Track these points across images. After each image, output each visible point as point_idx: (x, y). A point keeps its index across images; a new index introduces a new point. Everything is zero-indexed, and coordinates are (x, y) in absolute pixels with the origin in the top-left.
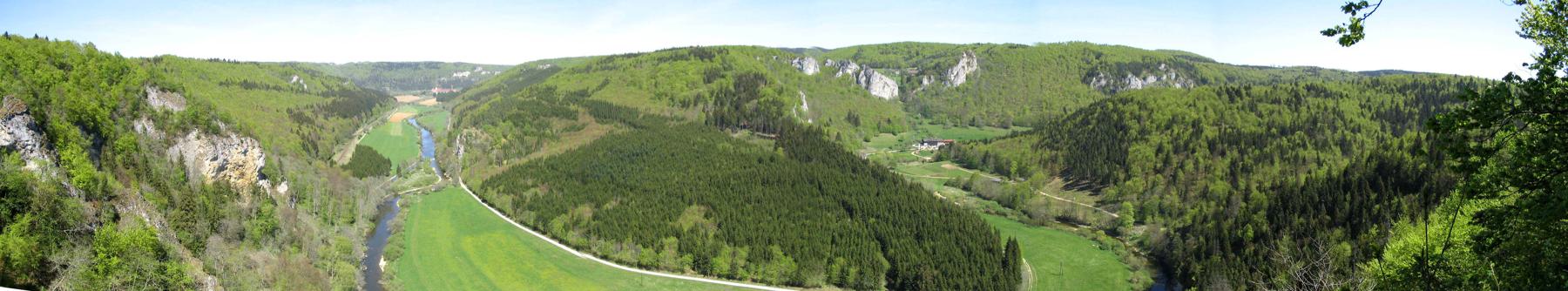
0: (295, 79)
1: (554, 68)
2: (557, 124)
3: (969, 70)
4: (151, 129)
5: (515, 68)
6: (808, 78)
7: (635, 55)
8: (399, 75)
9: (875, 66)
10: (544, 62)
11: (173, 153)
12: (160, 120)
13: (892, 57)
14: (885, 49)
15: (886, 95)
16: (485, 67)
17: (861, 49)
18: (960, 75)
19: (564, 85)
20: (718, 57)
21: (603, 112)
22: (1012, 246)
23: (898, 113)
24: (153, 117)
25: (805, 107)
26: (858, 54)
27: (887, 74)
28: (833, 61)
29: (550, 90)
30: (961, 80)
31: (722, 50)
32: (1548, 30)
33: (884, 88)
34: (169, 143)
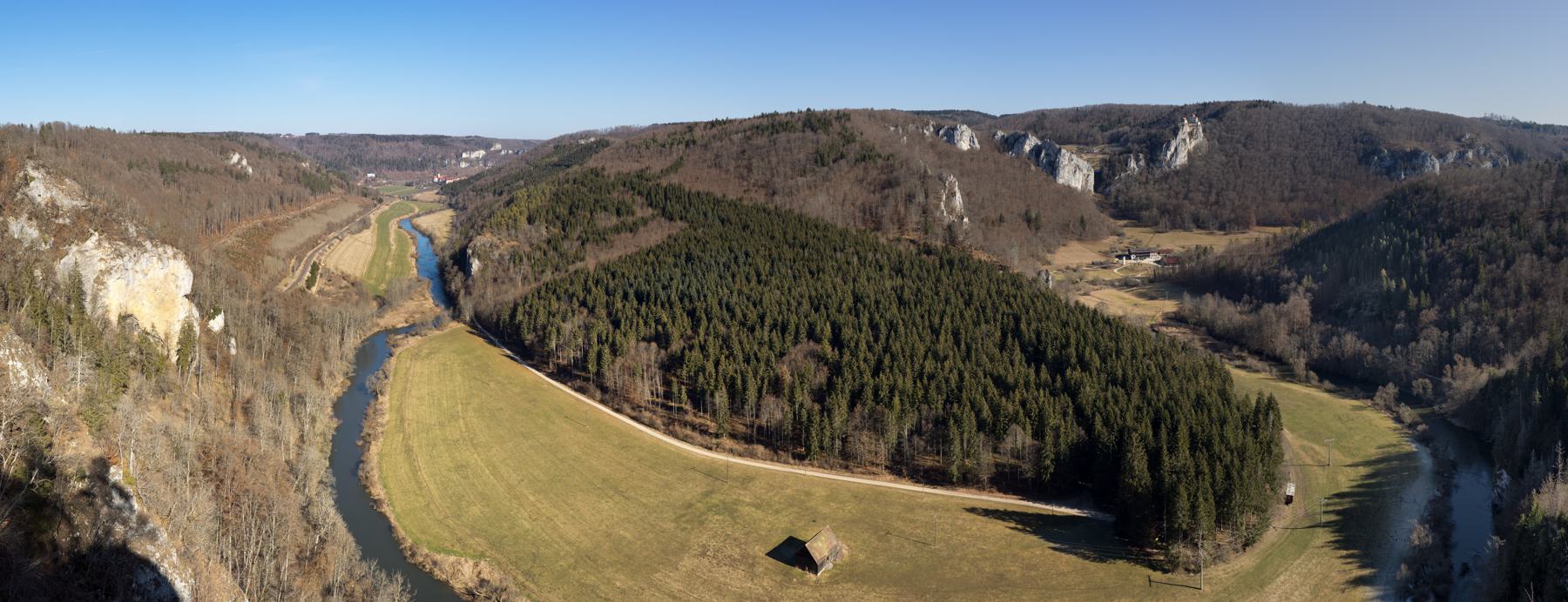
0: (236, 158)
1: (600, 143)
2: (606, 221)
3: (1191, 145)
4: (33, 233)
5: (545, 144)
6: (962, 154)
7: (724, 122)
8: (390, 152)
9: (1066, 141)
10: (586, 135)
11: (63, 266)
12: (44, 216)
13: (1083, 126)
14: (1077, 115)
15: (1077, 183)
16: (506, 143)
17: (1042, 116)
18: (1184, 147)
19: (614, 167)
20: (836, 126)
21: (666, 201)
22: (1268, 407)
23: (1091, 210)
24: (36, 215)
25: (958, 200)
26: (1038, 121)
27: (1079, 152)
28: (1006, 136)
29: (596, 173)
30: (1182, 159)
31: (843, 116)
32: (302, 291)
33: (1076, 172)
34: (58, 252)
